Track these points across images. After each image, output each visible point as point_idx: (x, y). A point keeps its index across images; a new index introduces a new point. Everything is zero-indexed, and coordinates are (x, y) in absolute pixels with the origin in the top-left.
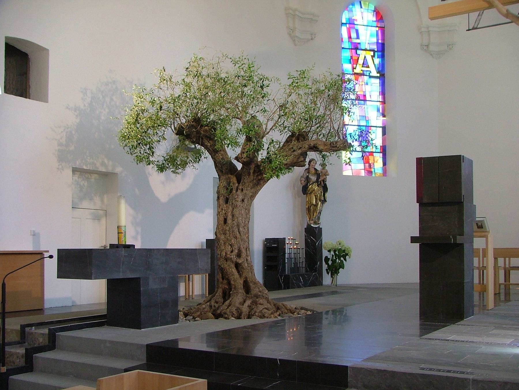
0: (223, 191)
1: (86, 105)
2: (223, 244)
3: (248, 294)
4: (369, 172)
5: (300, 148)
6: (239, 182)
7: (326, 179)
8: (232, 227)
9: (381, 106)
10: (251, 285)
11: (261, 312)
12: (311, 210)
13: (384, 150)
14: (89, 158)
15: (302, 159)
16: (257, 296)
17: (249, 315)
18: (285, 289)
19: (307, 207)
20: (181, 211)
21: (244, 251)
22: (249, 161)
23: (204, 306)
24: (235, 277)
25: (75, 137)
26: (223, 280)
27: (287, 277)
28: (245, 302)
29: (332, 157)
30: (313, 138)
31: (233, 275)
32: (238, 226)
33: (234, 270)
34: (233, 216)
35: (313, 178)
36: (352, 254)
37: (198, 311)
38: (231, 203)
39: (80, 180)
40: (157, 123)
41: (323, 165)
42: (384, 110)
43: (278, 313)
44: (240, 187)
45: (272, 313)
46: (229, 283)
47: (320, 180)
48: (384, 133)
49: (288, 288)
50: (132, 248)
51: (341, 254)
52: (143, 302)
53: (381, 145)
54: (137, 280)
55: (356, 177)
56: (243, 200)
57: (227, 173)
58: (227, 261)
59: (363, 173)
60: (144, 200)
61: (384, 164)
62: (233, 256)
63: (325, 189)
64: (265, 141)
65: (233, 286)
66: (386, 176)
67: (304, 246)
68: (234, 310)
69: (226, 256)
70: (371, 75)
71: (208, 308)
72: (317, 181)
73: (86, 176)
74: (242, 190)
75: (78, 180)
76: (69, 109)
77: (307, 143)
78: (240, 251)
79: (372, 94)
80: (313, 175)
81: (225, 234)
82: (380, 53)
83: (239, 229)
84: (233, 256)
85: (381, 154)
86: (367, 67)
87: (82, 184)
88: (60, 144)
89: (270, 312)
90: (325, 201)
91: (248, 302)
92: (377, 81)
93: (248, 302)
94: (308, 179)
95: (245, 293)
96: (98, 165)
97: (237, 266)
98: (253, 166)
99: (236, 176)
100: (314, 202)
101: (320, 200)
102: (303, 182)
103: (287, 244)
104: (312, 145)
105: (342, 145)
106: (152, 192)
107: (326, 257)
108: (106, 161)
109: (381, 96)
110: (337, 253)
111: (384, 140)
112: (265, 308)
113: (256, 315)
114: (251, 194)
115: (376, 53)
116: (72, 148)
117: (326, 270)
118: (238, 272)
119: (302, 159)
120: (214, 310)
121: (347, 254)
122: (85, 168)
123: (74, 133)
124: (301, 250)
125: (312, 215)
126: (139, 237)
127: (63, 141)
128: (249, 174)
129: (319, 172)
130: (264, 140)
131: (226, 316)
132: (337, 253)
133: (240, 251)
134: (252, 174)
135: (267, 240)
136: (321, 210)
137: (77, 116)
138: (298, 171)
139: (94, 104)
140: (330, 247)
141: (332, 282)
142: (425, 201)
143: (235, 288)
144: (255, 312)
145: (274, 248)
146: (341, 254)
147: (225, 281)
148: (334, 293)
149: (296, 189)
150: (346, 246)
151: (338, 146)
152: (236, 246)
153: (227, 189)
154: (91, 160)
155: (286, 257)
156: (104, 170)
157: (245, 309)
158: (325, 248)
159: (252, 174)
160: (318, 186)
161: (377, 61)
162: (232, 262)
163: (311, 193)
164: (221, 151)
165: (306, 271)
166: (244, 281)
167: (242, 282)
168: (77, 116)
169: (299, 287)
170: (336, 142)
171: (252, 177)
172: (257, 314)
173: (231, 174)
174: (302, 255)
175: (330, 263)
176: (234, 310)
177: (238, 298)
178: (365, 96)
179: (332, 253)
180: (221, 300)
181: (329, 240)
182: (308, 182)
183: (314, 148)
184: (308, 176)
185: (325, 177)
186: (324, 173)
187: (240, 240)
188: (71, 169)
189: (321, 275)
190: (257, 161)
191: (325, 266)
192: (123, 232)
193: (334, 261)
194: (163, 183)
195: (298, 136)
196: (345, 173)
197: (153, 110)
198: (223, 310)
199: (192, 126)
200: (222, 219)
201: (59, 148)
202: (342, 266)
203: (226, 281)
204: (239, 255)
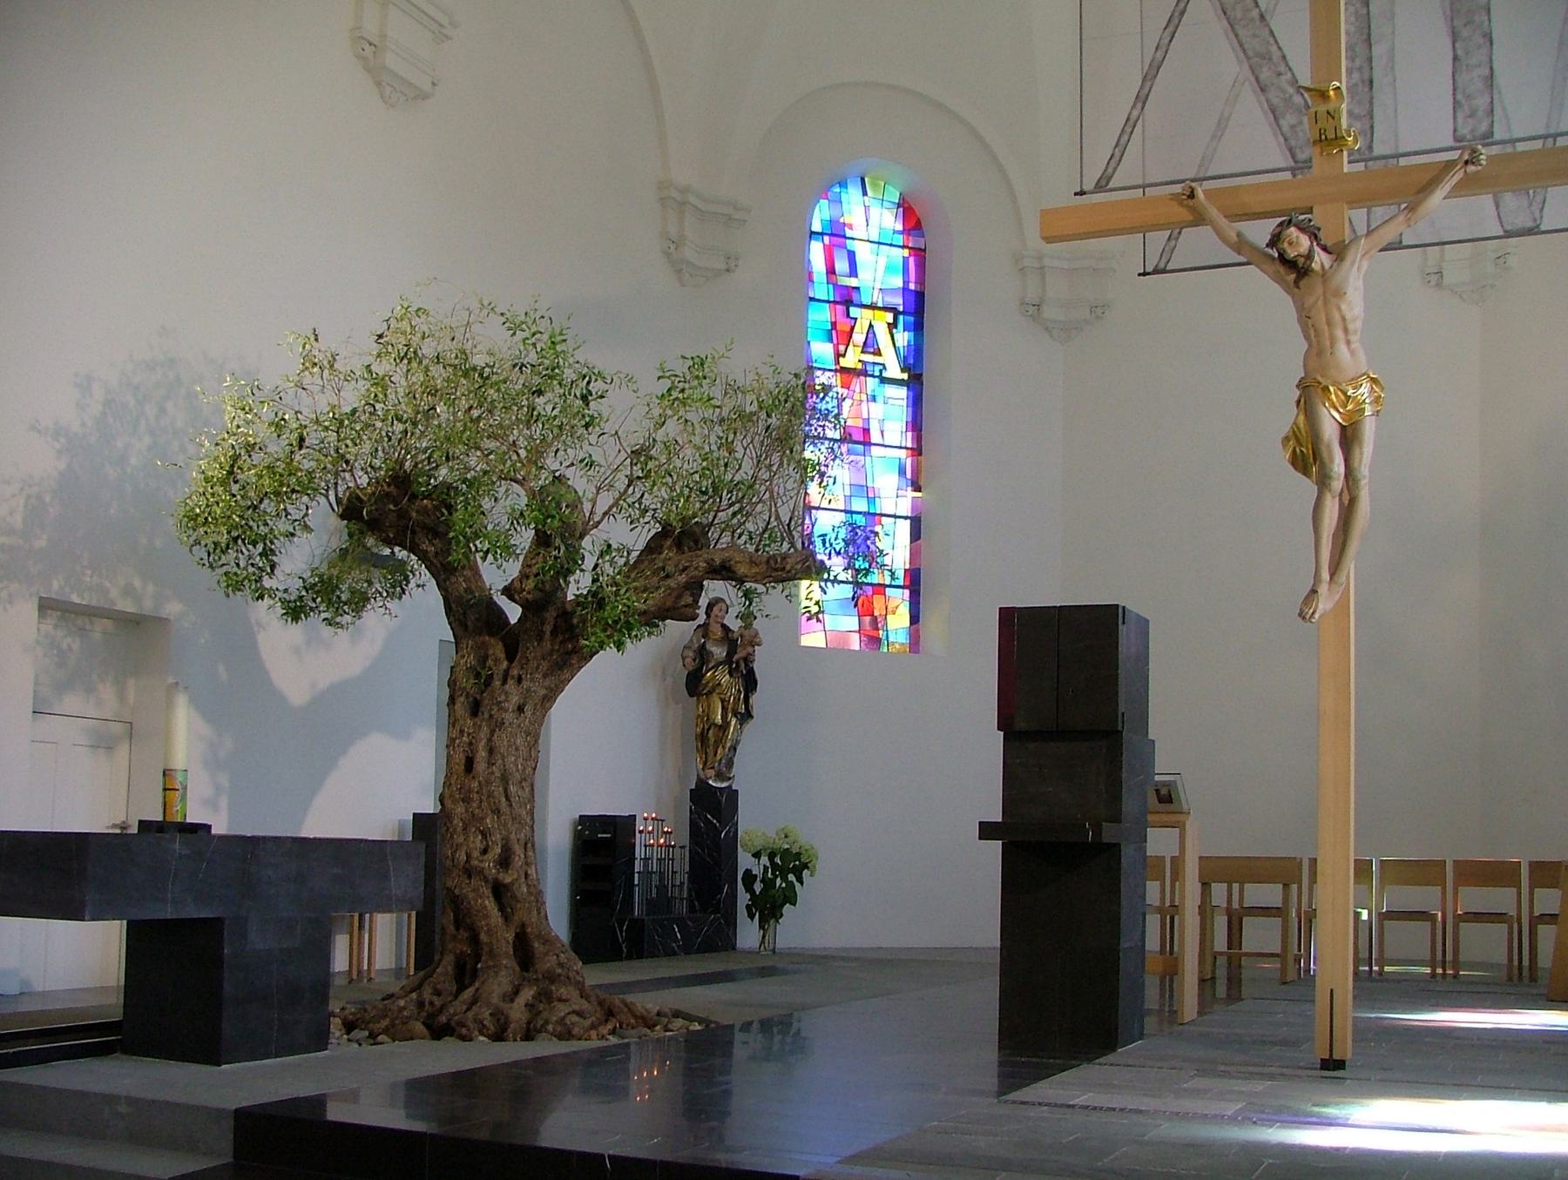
1: (89, 423)
3: (527, 971)
4: (873, 639)
5: (685, 569)
6: (511, 658)
8: (489, 783)
9: (909, 462)
11: (561, 1021)
12: (710, 742)
13: (913, 581)
15: (690, 600)
16: (551, 978)
17: (528, 1029)
18: (630, 957)
20: (348, 736)
22: (541, 598)
23: (402, 1003)
27: (637, 927)
28: (516, 992)
29: (770, 599)
31: (486, 916)
32: (505, 779)
33: (490, 904)
35: (719, 652)
36: (819, 865)
38: (486, 716)
39: (60, 633)
40: (288, 484)
43: (610, 1026)
44: (515, 672)
45: (593, 1027)
46: (475, 940)
48: (916, 535)
49: (640, 956)
50: (201, 833)
51: (790, 864)
52: (228, 989)
54: (212, 927)
55: (834, 652)
56: (520, 709)
58: (470, 877)
59: (855, 643)
60: (241, 697)
61: (914, 619)
62: (489, 864)
63: (750, 683)
65: (486, 949)
66: (917, 652)
67: (685, 839)
70: (885, 374)
73: (79, 622)
74: (520, 680)
79: (887, 426)
81: (467, 800)
82: (911, 319)
83: (506, 790)
84: (489, 864)
85: (907, 592)
87: (65, 646)
90: (748, 715)
91: (528, 994)
92: (902, 392)
93: (528, 994)
94: (702, 654)
96: (114, 593)
98: (550, 615)
99: (502, 640)
101: (735, 714)
107: (748, 872)
108: (137, 583)
109: (910, 434)
111: (915, 554)
112: (573, 1012)
114: (544, 692)
116: (41, 543)
118: (502, 909)
119: (690, 600)
120: (431, 1016)
121: (806, 866)
122: (75, 599)
123: (48, 499)
124: (677, 850)
125: (710, 751)
126: (224, 803)
128: (540, 637)
130: (586, 542)
131: (464, 1031)
135: (583, 819)
136: (738, 742)
138: (677, 632)
140: (758, 844)
141: (763, 942)
144: (547, 1022)
145: (602, 842)
146: (790, 864)
147: (464, 934)
148: (766, 972)
149: (669, 680)
153: (478, 676)
156: (127, 606)
157: (517, 1012)
161: (903, 338)
163: (710, 693)
164: (463, 568)
165: (692, 909)
166: (517, 935)
167: (510, 936)
170: (785, 557)
171: (547, 645)
172: (550, 1027)
173: (491, 634)
174: (681, 865)
175: (758, 887)
177: (498, 982)
178: (866, 431)
179: (765, 860)
181: (756, 824)
183: (723, 571)
185: (750, 649)
188: (36, 601)
189: (732, 923)
191: (743, 898)
193: (768, 884)
195: (680, 537)
196: (806, 641)
198: (455, 1014)
199: (388, 494)
200: (460, 758)
204: (505, 862)
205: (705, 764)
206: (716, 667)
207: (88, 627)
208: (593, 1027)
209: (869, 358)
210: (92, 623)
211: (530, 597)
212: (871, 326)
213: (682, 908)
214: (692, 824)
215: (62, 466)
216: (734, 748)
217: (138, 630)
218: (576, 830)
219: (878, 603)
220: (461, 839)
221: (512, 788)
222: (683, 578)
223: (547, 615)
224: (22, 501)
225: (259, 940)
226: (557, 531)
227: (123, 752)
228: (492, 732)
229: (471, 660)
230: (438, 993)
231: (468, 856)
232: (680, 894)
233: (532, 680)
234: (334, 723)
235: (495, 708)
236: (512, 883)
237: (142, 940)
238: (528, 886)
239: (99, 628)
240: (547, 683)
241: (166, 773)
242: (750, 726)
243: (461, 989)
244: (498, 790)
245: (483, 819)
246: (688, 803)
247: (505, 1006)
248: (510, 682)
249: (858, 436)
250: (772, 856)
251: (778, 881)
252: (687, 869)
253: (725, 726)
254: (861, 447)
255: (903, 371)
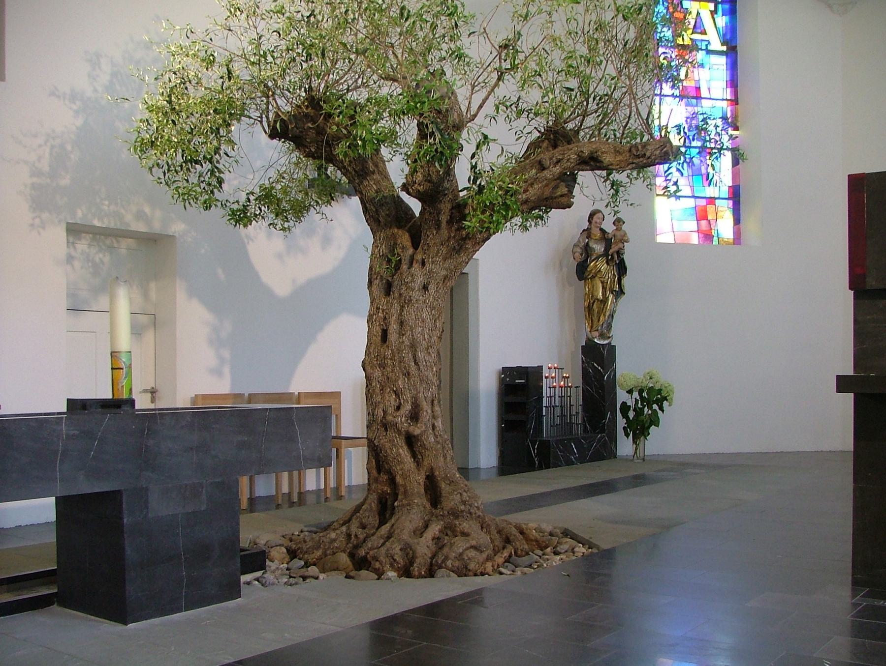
0: (382, 269)
1: (100, 89)
2: (378, 391)
3: (436, 508)
4: (707, 236)
5: (559, 161)
6: (415, 245)
7: (622, 249)
8: (400, 351)
9: (729, 109)
10: (443, 485)
11: (460, 556)
12: (595, 312)
13: (735, 194)
14: (107, 203)
15: (565, 190)
16: (455, 514)
17: (431, 564)
18: (540, 468)
19: (586, 304)
20: (287, 315)
21: (426, 406)
22: (435, 190)
23: (333, 535)
24: (406, 467)
25: (72, 156)
26: (379, 473)
27: (545, 446)
28: (426, 526)
29: (634, 188)
30: (585, 143)
31: (400, 462)
32: (413, 347)
33: (404, 452)
34: (401, 323)
35: (599, 248)
36: (676, 397)
37: (318, 548)
38: (397, 295)
39: (93, 250)
40: (227, 112)
41: (618, 222)
42: (735, 116)
43: (506, 554)
44: (419, 257)
45: (488, 559)
46: (392, 481)
47: (611, 252)
48: (736, 162)
49: (548, 467)
50: (125, 408)
51: (654, 398)
52: (130, 552)
53: (731, 184)
54: (114, 497)
55: (679, 248)
56: (425, 288)
57: (389, 225)
58: (386, 430)
59: (695, 239)
60: (235, 293)
61: (737, 221)
62: (401, 419)
63: (622, 269)
64: (468, 140)
65: (402, 489)
66: (739, 243)
67: (579, 381)
68: (396, 549)
69: (384, 417)
70: (710, 48)
71: (341, 542)
72: (606, 254)
73: (108, 242)
74: (423, 264)
75: (87, 250)
76: (59, 97)
77: (574, 147)
78: (416, 406)
79: (713, 85)
80: (597, 241)
81: (383, 366)
82: (727, 6)
83: (414, 357)
84: (401, 419)
85: (731, 202)
86: (702, 33)
87: (97, 259)
88: (36, 173)
89: (484, 556)
90: (621, 292)
91: (435, 529)
92: (723, 60)
93: (435, 529)
94: (587, 249)
95: (428, 506)
96: (129, 218)
97: (411, 441)
98: (445, 207)
99: (409, 231)
100: (600, 295)
101: (612, 292)
102: (577, 254)
103: (546, 378)
104: (586, 153)
105: (657, 152)
106: (256, 276)
107: (624, 404)
108: (147, 210)
109: (729, 90)
110: (645, 394)
111: (735, 176)
112: (472, 547)
113: (447, 568)
114: (444, 273)
115: (720, 6)
116: (65, 181)
117: (624, 428)
118: (414, 455)
119: (565, 190)
120: (357, 547)
121: (665, 399)
122: (97, 223)
123: (69, 148)
124: (573, 389)
125: (595, 319)
126: (227, 370)
127: (45, 165)
128: (438, 226)
129: (610, 236)
130: (464, 134)
131: (377, 565)
132: (645, 394)
133: (416, 406)
134: (444, 224)
135: (505, 370)
136: (614, 311)
137: (77, 112)
139: (118, 87)
140: (631, 384)
141: (636, 453)
142: (872, 283)
143: (405, 492)
144: (447, 558)
145: (519, 388)
146: (654, 398)
147: (384, 477)
148: (638, 480)
149: (565, 269)
150: (662, 381)
151: (648, 154)
152: (408, 396)
153: (389, 261)
154: (112, 207)
155: (544, 405)
156: (141, 228)
157: (424, 547)
158: (621, 386)
159: (444, 224)
160: (608, 264)
161: (722, 21)
162: (399, 432)
163: (593, 277)
164: (373, 173)
165: (585, 430)
166: (428, 477)
167: (421, 478)
168: (77, 112)
169: (569, 463)
170: (644, 146)
171: (444, 232)
172: (449, 563)
173: (399, 227)
174: (577, 400)
175: (631, 414)
176: (398, 549)
177: (410, 517)
178: (698, 89)
179: (636, 395)
180: (374, 520)
181: (629, 370)
182: (588, 256)
183: (592, 162)
184: (588, 244)
185: (621, 245)
186: (619, 237)
187: (417, 379)
188: (64, 226)
189: (613, 439)
190: (456, 191)
191: (621, 422)
192: (123, 366)
193: (639, 412)
194: (280, 256)
195: (556, 136)
197: (213, 77)
198: (371, 549)
199: (306, 116)
200: (377, 330)
201: (35, 180)
202: (654, 421)
203: (386, 477)
204: (415, 416)
205: (592, 327)
206: (597, 258)
207: (116, 245)
208: (488, 559)
209: (696, 37)
210: (118, 242)
211: (421, 188)
212: (698, 13)
213: (579, 431)
214: (584, 371)
215: (79, 122)
216: (612, 316)
217: (154, 244)
218: (500, 376)
219: (710, 208)
220: (379, 399)
221: (420, 355)
222: (557, 170)
223: (442, 206)
224: (48, 151)
225: (162, 506)
226: (441, 127)
227: (149, 336)
228: (402, 307)
229: (384, 249)
230: (363, 527)
231: (385, 412)
232: (578, 422)
233: (433, 262)
234: (307, 310)
235: (404, 288)
236: (421, 434)
237: (62, 503)
238: (436, 436)
239: (125, 244)
240: (446, 265)
241: (114, 355)
242: (623, 298)
243: (382, 523)
244: (408, 356)
245: (396, 381)
246: (580, 356)
247: (412, 541)
248: (415, 265)
249: (693, 93)
250: (641, 392)
251: (646, 409)
252: (581, 402)
253: (604, 301)
254: (694, 101)
255: (722, 45)
